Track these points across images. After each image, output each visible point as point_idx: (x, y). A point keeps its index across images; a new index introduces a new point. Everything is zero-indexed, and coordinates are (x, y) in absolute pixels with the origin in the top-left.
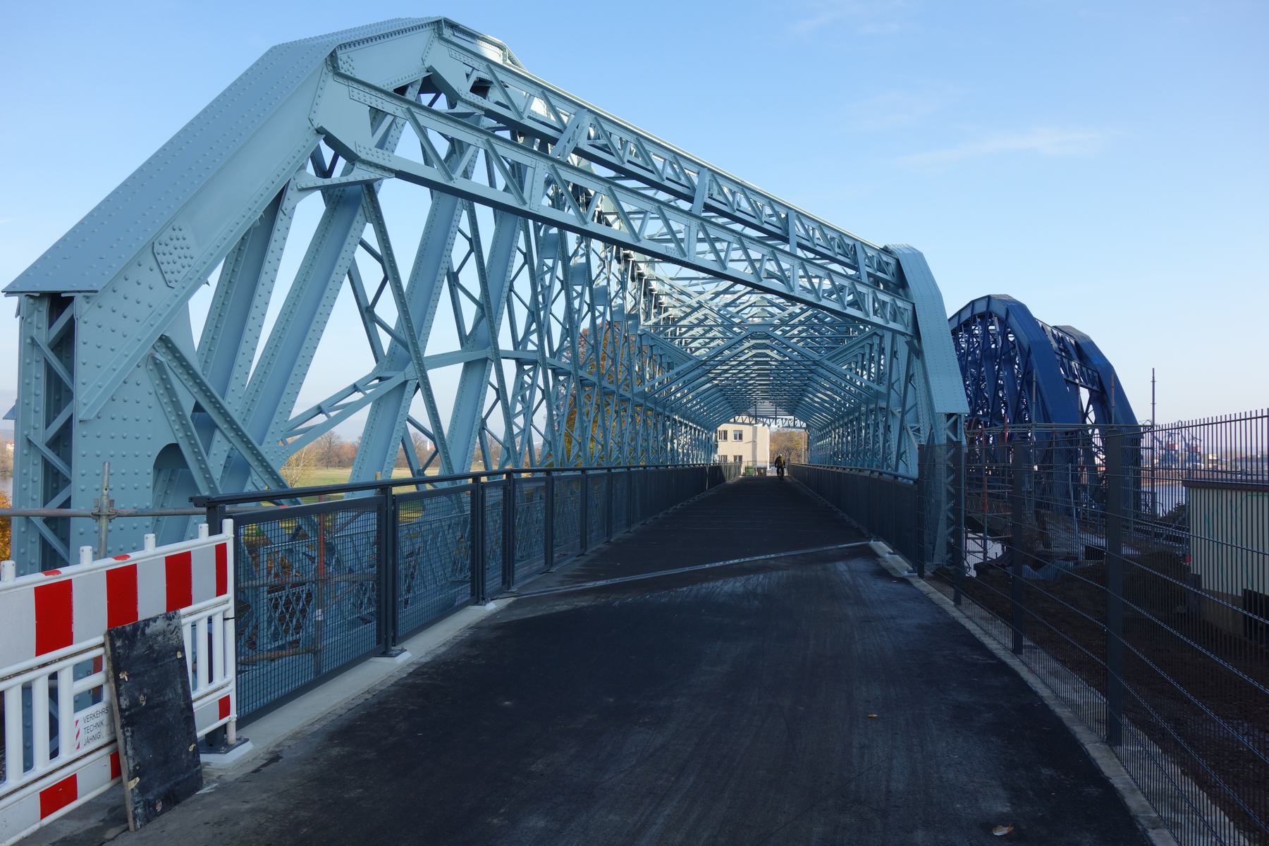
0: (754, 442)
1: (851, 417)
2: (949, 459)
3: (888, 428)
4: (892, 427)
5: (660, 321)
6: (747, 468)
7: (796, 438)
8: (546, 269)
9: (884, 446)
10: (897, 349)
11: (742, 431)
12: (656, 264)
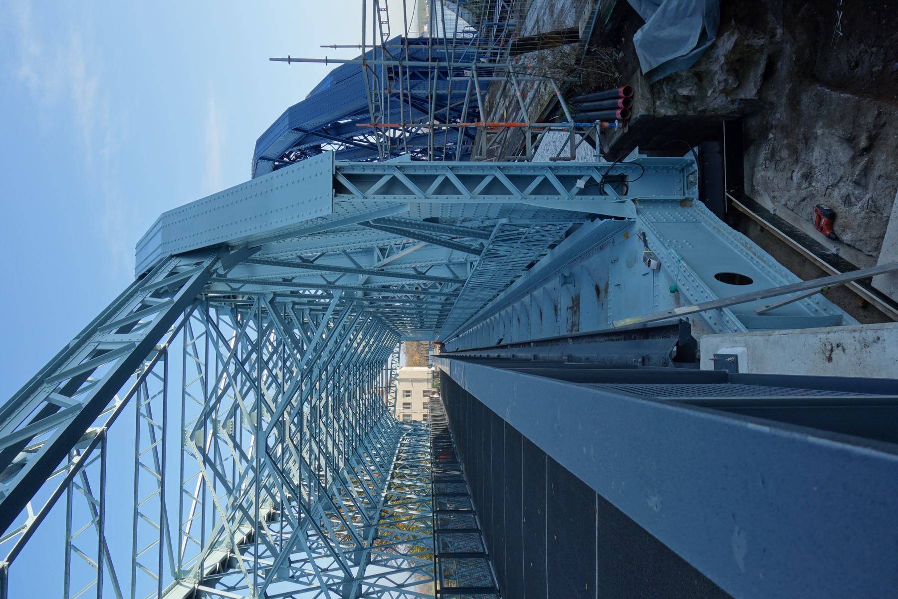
0: (412, 381)
1: (383, 318)
2: (424, 191)
3: (386, 288)
10: (281, 278)
11: (403, 391)
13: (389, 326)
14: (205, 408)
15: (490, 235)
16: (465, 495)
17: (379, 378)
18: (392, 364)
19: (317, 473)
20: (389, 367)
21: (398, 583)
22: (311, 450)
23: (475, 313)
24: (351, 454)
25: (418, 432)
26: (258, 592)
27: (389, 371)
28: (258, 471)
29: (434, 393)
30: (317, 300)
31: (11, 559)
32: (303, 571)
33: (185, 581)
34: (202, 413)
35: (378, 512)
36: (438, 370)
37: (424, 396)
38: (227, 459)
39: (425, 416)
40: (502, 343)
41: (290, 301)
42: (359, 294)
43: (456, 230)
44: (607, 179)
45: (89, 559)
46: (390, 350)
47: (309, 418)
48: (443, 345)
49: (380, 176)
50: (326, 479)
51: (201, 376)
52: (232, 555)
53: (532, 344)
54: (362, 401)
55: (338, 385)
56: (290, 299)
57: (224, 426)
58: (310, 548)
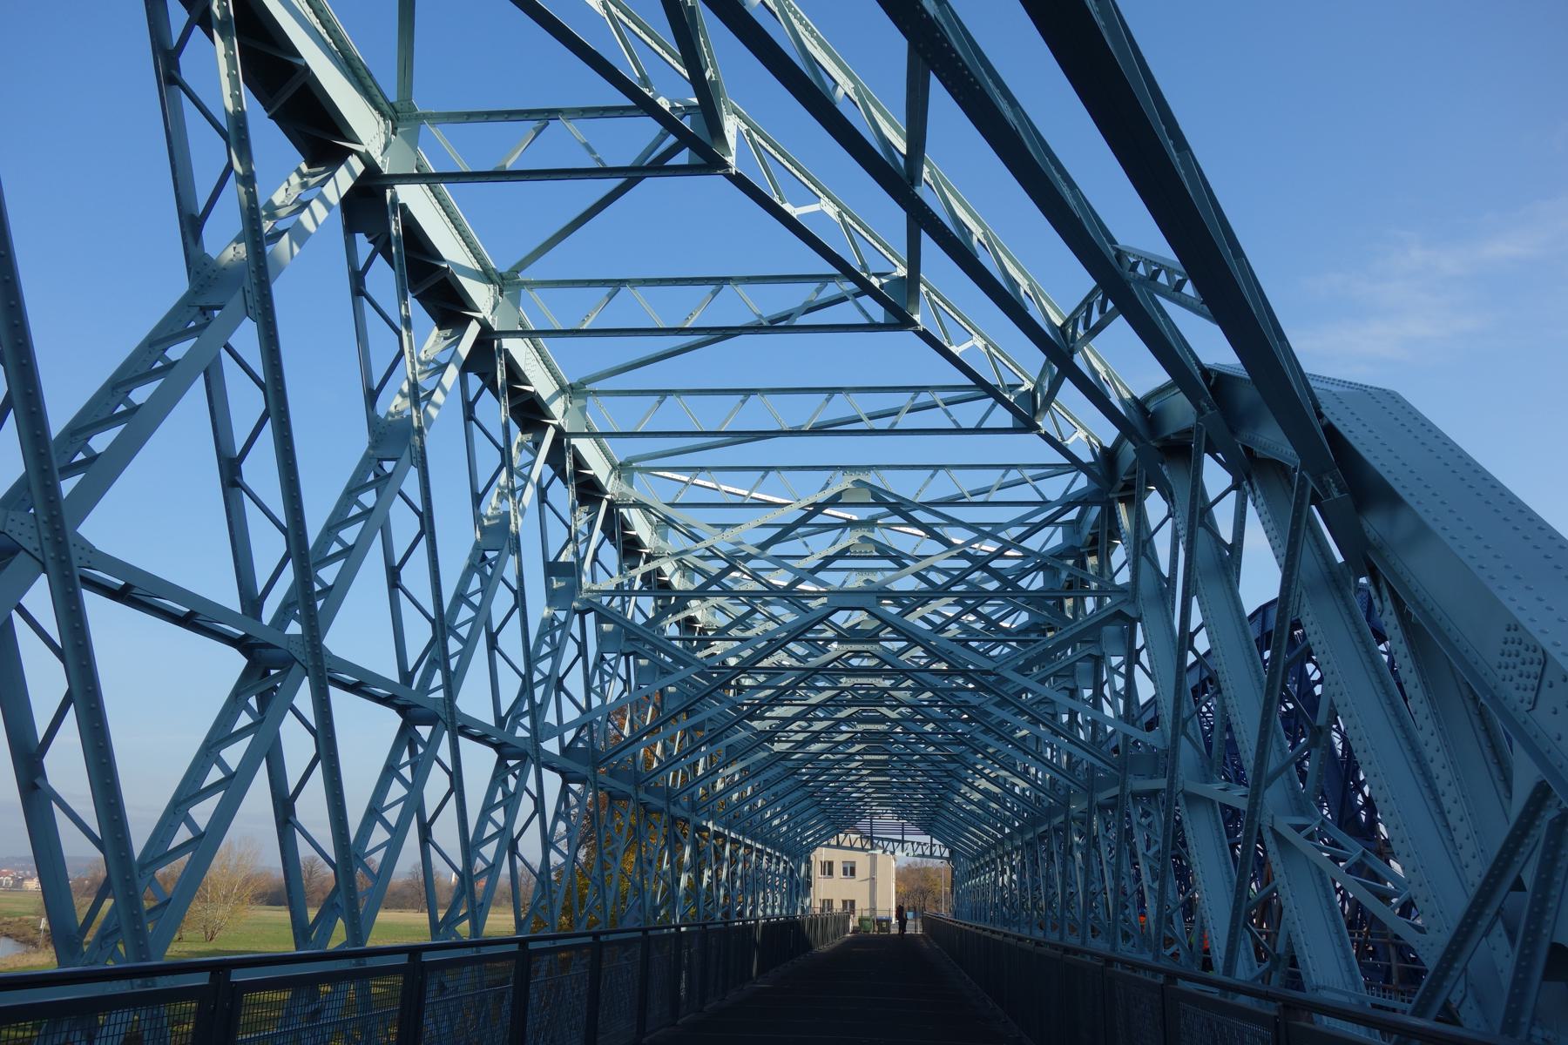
0: (873, 880)
5: (632, 581)
6: (861, 920)
7: (933, 877)
8: (556, 623)
11: (854, 862)
12: (636, 474)
14: (911, 502)
18: (913, 843)
20: (907, 838)
21: (433, 828)
25: (794, 891)
26: (594, 597)
27: (900, 837)
28: (789, 595)
31: (740, 182)
32: (612, 676)
33: (615, 479)
34: (904, 499)
35: (685, 815)
37: (844, 902)
38: (807, 545)
45: (697, 315)
51: (967, 495)
52: (644, 556)
57: (864, 539)
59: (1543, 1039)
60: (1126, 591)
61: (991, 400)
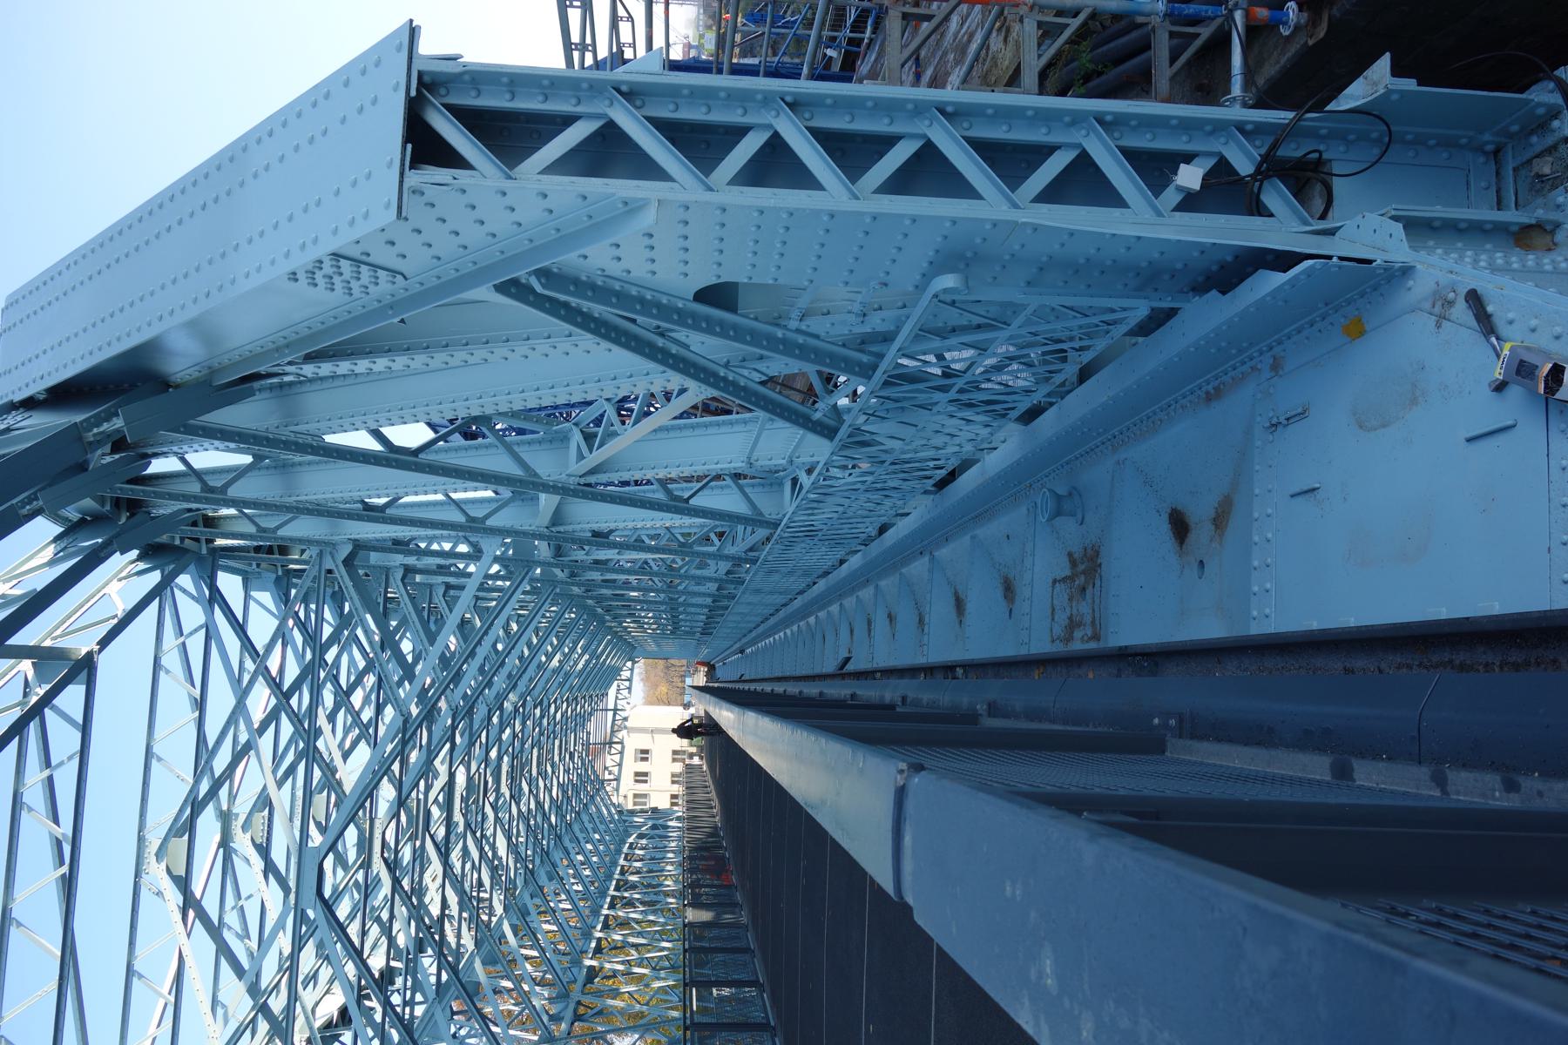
1: (599, 610)
4: (595, 527)
9: (650, 549)
13: (611, 627)
15: (874, 368)
16: (746, 950)
17: (591, 726)
18: (617, 698)
19: (475, 894)
20: (611, 706)
22: (465, 852)
23: (785, 605)
24: (538, 861)
27: (610, 714)
29: (691, 756)
30: (490, 582)
35: (572, 1006)
36: (702, 713)
37: (674, 760)
39: (674, 797)
40: (850, 667)
41: (397, 563)
42: (543, 550)
43: (784, 341)
44: (1271, 167)
46: (614, 673)
47: (464, 794)
48: (711, 668)
49: (567, 121)
50: (491, 907)
53: (960, 671)
54: (544, 780)
55: (520, 735)
56: (440, 579)
58: (454, 1036)
59: (801, 320)
60: (321, 551)
61: (47, 710)
